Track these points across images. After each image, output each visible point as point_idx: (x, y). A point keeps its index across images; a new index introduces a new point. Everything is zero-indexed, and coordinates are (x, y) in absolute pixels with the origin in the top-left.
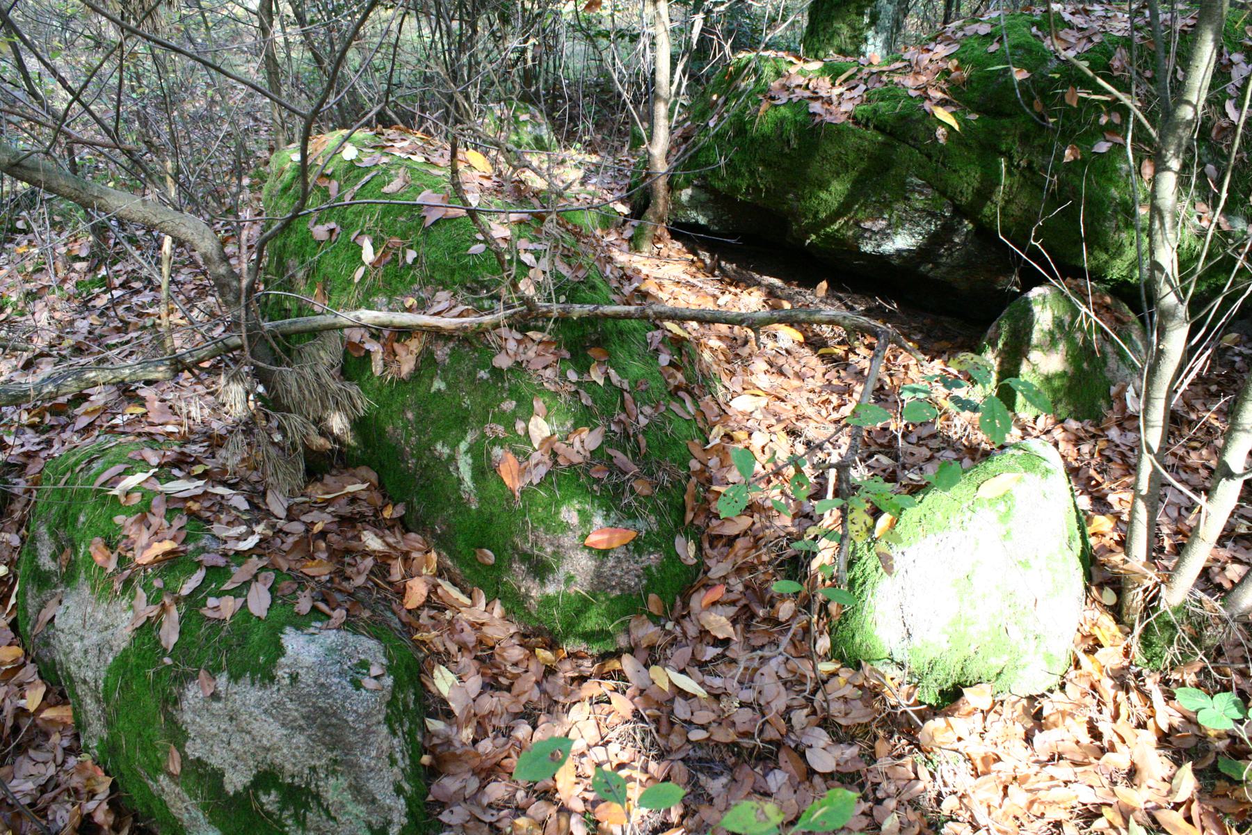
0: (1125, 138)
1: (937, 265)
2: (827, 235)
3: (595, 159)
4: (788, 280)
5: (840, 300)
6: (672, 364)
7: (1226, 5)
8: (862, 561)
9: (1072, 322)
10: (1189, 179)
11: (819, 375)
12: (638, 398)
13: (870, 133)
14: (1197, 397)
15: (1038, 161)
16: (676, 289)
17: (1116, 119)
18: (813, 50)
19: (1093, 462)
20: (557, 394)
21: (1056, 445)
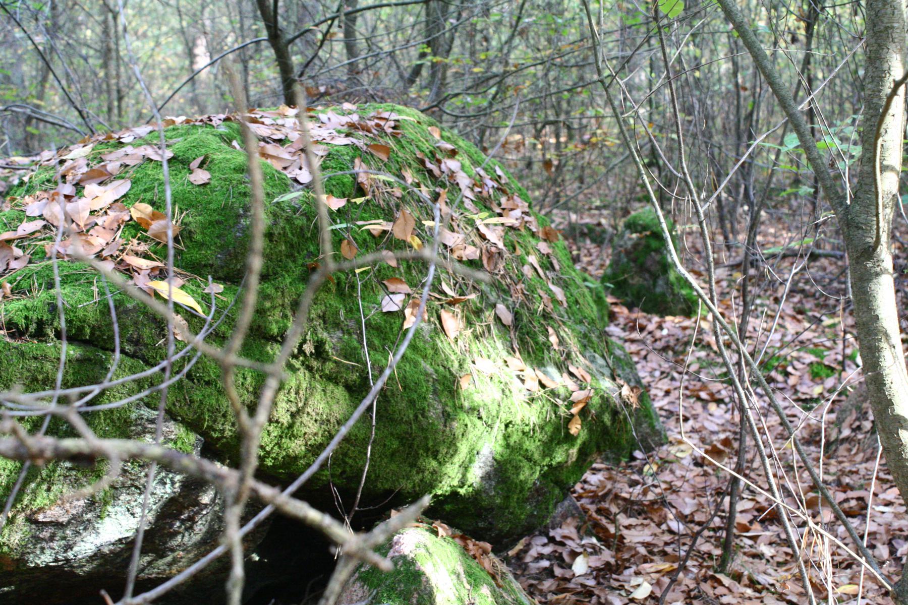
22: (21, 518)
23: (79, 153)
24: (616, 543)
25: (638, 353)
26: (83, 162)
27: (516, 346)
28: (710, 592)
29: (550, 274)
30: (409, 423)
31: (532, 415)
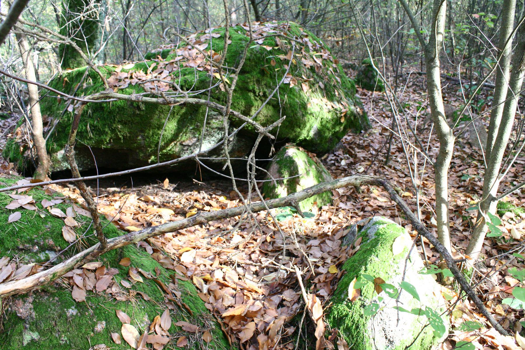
8: (350, 316)
20: (128, 301)
22: (178, 144)
23: (193, 37)
24: (355, 156)
25: (364, 102)
26: (194, 39)
27: (325, 95)
28: (382, 171)
29: (336, 74)
30: (291, 117)
31: (329, 116)
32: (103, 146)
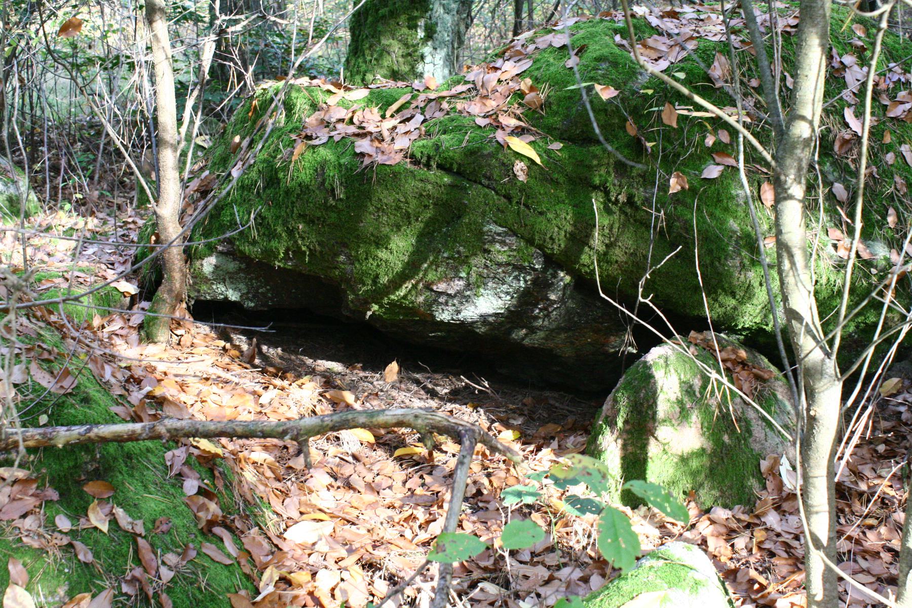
0: (737, 161)
1: (532, 330)
2: (392, 304)
3: (92, 223)
4: (349, 362)
5: (418, 382)
6: (201, 492)
7: (828, 5)
9: (704, 387)
10: (816, 201)
11: (398, 484)
12: (158, 543)
13: (434, 174)
14: (863, 461)
15: (640, 194)
16: (205, 388)
17: (725, 137)
18: (358, 72)
19: (752, 560)
20: (42, 551)
21: (703, 544)
32: (276, 263)
